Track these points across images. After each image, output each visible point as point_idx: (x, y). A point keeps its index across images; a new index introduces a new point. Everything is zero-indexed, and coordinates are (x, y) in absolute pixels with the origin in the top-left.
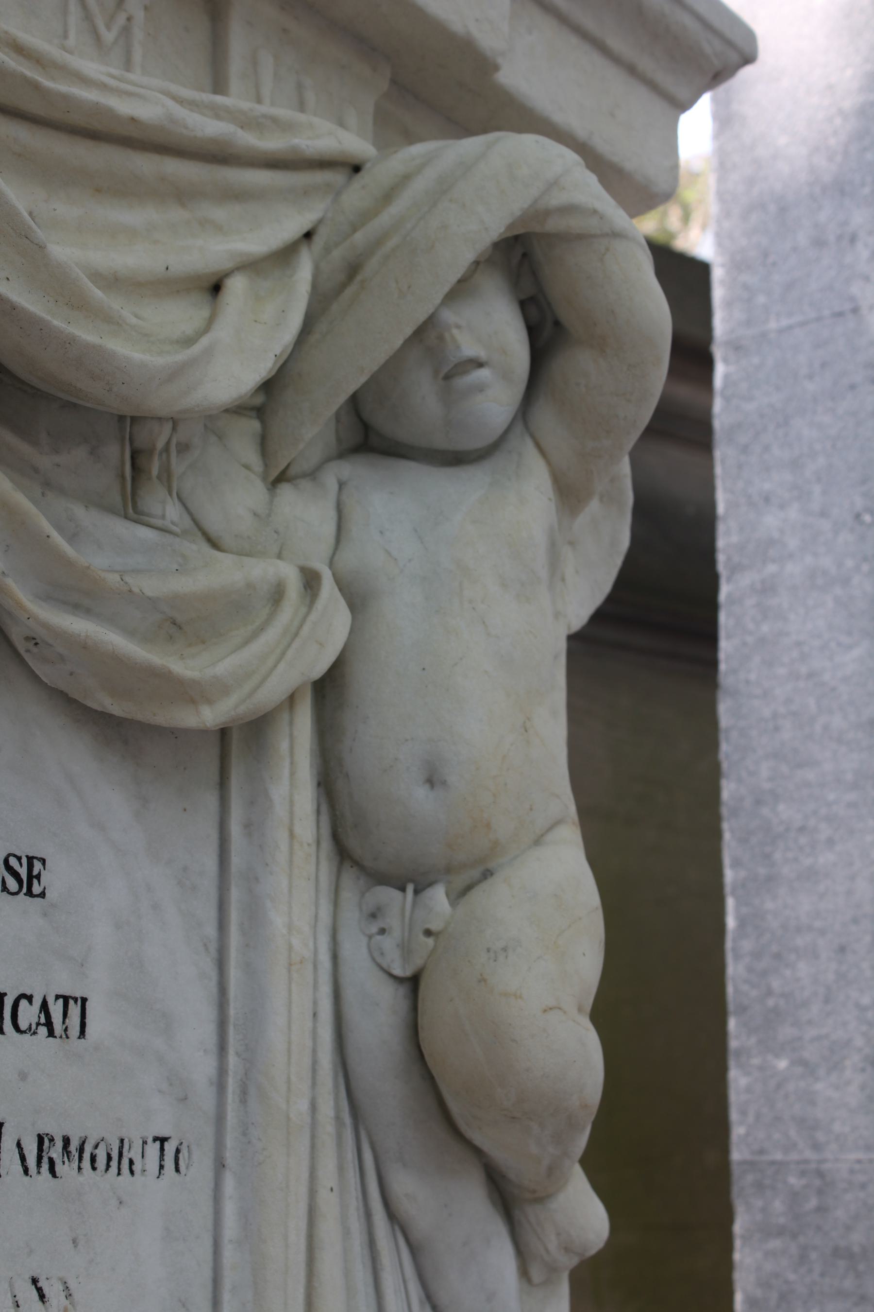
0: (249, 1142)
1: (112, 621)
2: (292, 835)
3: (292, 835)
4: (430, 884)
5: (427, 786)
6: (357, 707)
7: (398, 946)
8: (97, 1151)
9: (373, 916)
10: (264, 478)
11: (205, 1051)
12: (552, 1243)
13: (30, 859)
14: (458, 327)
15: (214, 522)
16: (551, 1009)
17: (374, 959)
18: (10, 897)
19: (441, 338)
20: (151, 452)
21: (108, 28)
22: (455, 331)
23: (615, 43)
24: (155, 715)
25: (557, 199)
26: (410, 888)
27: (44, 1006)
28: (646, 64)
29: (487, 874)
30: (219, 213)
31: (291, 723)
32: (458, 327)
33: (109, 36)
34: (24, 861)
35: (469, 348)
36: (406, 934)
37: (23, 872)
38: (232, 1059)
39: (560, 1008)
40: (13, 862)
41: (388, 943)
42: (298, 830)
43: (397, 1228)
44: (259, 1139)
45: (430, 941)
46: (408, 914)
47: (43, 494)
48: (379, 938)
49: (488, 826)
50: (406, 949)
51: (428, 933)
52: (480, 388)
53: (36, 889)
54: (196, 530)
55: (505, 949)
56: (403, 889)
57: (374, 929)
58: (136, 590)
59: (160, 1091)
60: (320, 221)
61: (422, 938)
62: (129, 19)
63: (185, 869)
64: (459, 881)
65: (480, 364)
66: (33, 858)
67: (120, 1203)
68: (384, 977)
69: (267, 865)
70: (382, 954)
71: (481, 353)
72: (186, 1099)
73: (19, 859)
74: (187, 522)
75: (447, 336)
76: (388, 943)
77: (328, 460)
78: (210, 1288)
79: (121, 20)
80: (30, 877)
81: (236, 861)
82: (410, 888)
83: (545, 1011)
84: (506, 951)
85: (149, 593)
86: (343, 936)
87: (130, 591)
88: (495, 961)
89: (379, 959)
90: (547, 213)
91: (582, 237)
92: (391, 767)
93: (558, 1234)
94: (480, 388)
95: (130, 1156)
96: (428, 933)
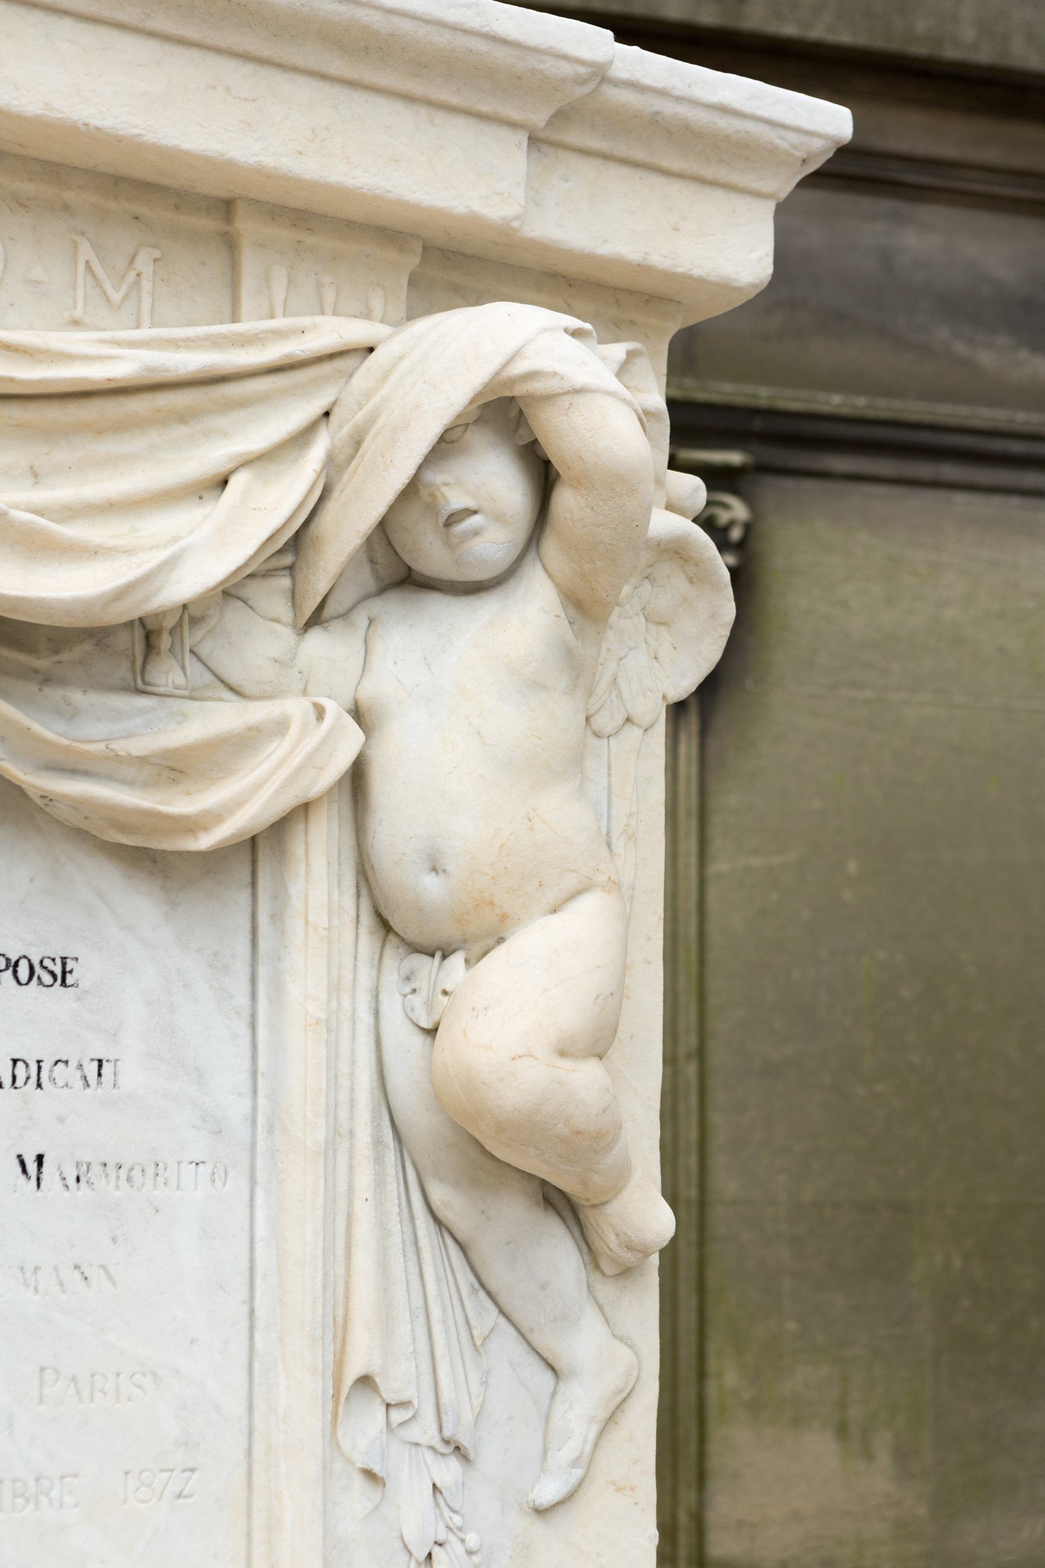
0: (275, 1165)
1: (108, 778)
2: (307, 922)
3: (307, 922)
4: (453, 952)
5: (434, 873)
6: (375, 811)
7: (425, 1003)
8: (133, 1173)
9: (408, 979)
10: (294, 626)
11: (239, 1094)
12: (612, 1241)
13: (64, 960)
14: (447, 484)
15: (233, 673)
16: (520, 1057)
17: (407, 1015)
18: (45, 989)
19: (433, 495)
20: (159, 632)
21: (117, 289)
22: (444, 489)
23: (666, 163)
24: (160, 842)
25: (520, 367)
26: (438, 955)
27: (80, 1066)
28: (710, 172)
29: (501, 940)
30: (222, 422)
31: (306, 831)
32: (447, 484)
33: (116, 296)
34: (58, 961)
35: (456, 500)
36: (431, 994)
37: (58, 971)
38: (262, 1101)
39: (531, 1056)
40: (47, 963)
41: (417, 1001)
42: (311, 918)
43: (443, 1229)
44: (282, 1162)
45: (445, 999)
46: (433, 977)
47: (40, 690)
48: (410, 996)
49: (491, 903)
50: (429, 1005)
51: (445, 993)
52: (476, 533)
53: (69, 980)
54: (218, 683)
55: (486, 1009)
56: (433, 955)
57: (408, 990)
58: (122, 753)
59: (194, 1127)
60: (335, 403)
61: (440, 997)
62: (138, 275)
63: (216, 954)
64: (477, 949)
65: (475, 512)
66: (66, 958)
67: (157, 1211)
68: (416, 1030)
69: (286, 947)
70: (412, 1010)
71: (471, 504)
72: (221, 1132)
73: (53, 960)
74: (208, 677)
75: (437, 493)
76: (417, 1002)
77: (366, 598)
78: (247, 1275)
79: (131, 276)
80: (64, 973)
81: (263, 944)
82: (438, 955)
83: (514, 1059)
84: (486, 1010)
85: (135, 753)
86: (384, 997)
87: (117, 755)
88: (476, 1018)
89: (411, 1015)
90: (512, 382)
91: (550, 398)
92: (401, 860)
93: (617, 1235)
94: (476, 533)
95: (165, 1176)
96: (445, 993)
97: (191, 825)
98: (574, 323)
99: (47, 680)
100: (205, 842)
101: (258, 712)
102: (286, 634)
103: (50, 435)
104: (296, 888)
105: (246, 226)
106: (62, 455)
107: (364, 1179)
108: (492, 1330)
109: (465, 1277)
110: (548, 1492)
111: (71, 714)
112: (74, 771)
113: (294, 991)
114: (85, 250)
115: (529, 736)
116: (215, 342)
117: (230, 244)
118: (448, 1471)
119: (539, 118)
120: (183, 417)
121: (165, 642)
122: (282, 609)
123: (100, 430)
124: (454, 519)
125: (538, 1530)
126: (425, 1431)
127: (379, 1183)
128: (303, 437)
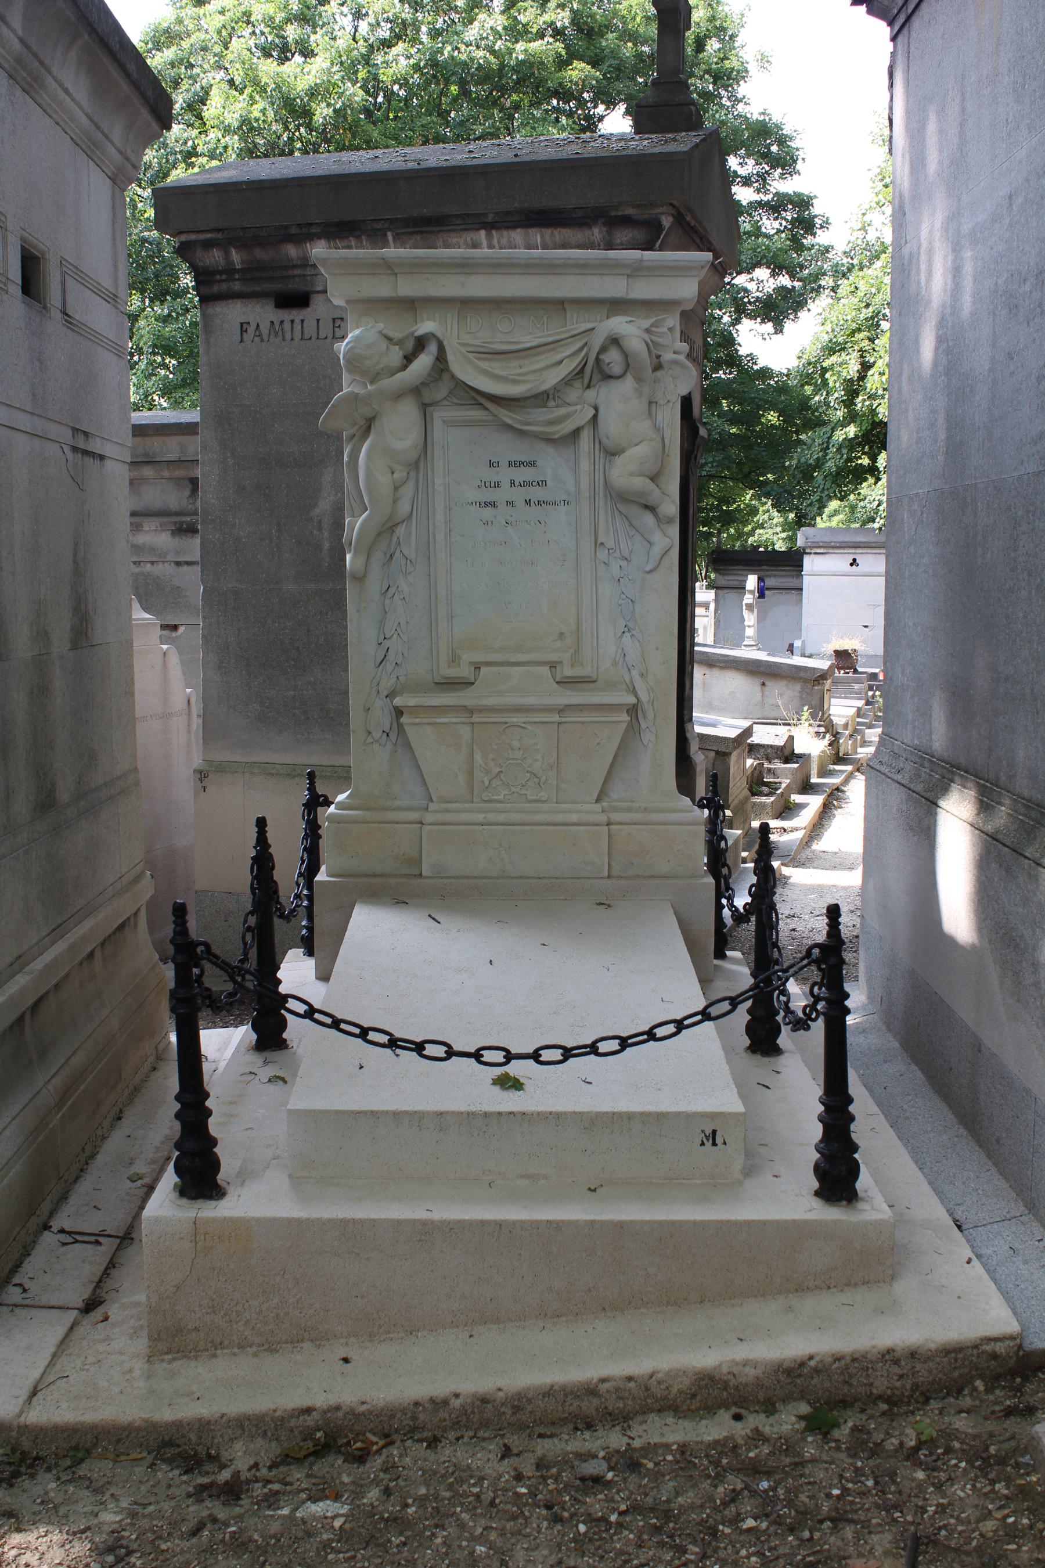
97: (554, 433)
98: (629, 319)
99: (523, 407)
100: (556, 436)
101: (570, 409)
102: (580, 392)
103: (523, 358)
104: (581, 444)
105: (566, 306)
106: (526, 361)
107: (602, 504)
108: (1014, 851)
109: (627, 523)
110: (648, 568)
111: (529, 414)
112: (529, 424)
113: (582, 465)
114: (532, 318)
115: (136, 358)
116: (559, 334)
117: (564, 310)
118: (624, 563)
119: (629, 272)
120: (552, 350)
121: (551, 396)
122: (580, 386)
123: (535, 355)
124: (609, 364)
125: (648, 576)
126: (618, 554)
127: (606, 504)
128: (581, 349)
